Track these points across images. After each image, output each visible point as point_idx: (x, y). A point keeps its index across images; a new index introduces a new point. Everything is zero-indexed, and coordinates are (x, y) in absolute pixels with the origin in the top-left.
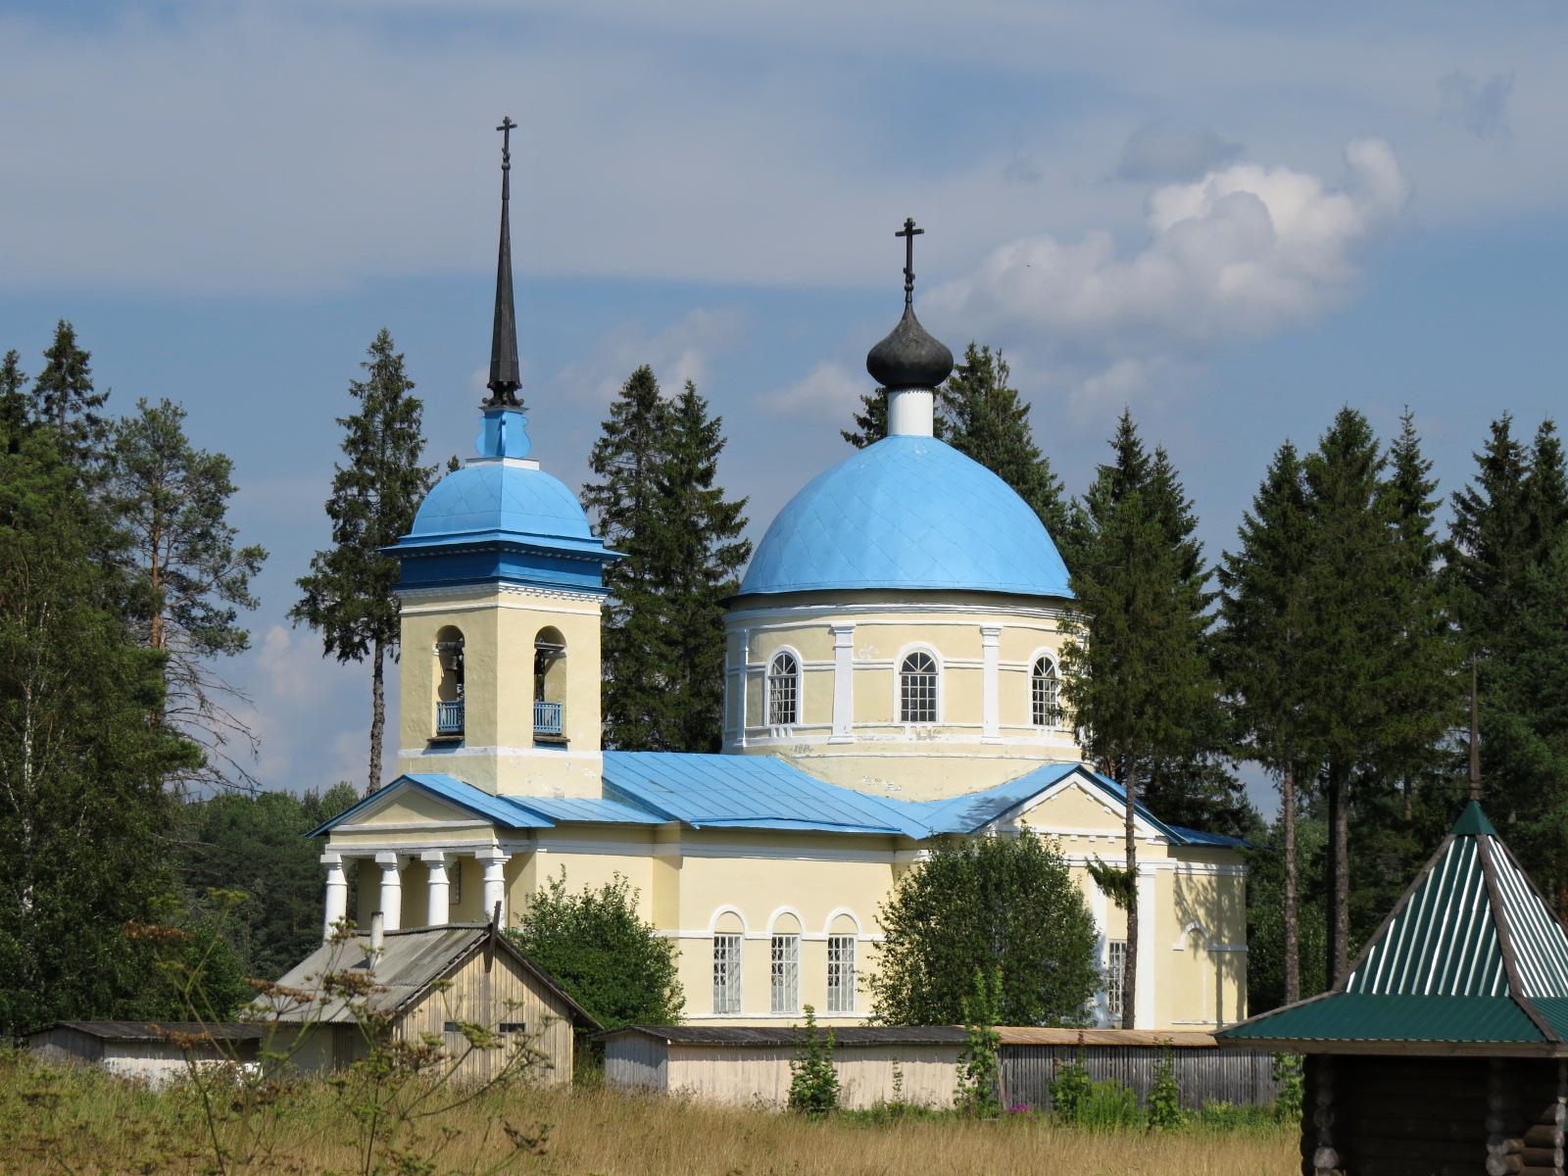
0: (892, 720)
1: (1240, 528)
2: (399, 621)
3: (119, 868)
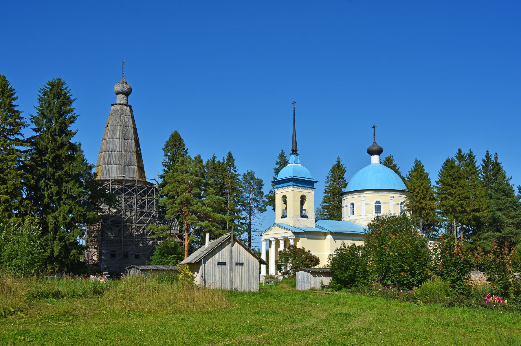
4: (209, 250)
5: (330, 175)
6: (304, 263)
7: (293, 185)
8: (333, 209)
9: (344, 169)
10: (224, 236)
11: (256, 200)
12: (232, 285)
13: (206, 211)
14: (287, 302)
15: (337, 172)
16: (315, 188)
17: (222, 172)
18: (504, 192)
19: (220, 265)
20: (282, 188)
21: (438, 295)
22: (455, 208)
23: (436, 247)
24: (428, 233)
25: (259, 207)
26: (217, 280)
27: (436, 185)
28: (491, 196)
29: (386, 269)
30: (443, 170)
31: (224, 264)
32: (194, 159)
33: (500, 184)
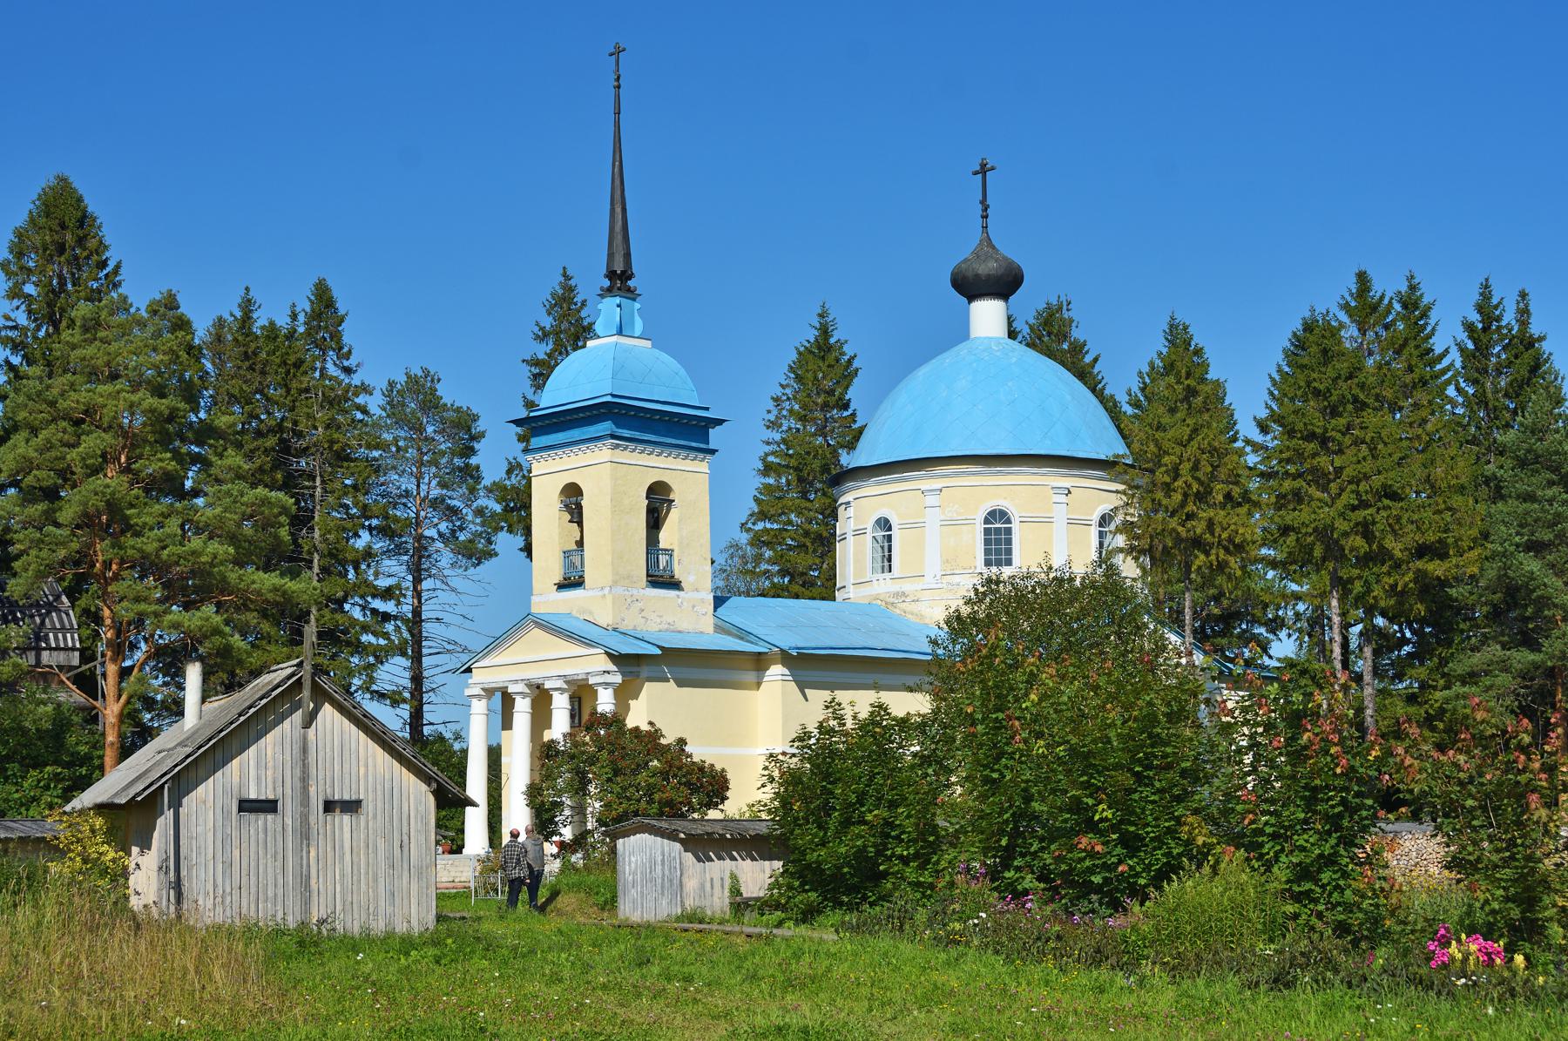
1: (1279, 366)
4: (199, 741)
5: (788, 391)
6: (656, 797)
7: (613, 437)
8: (802, 547)
9: (850, 362)
10: (272, 675)
11: (449, 508)
12: (306, 903)
13: (204, 559)
14: (556, 979)
15: (816, 378)
16: (713, 452)
17: (288, 373)
18: (1556, 470)
19: (251, 811)
20: (560, 452)
21: (1232, 935)
22: (1337, 542)
23: (1228, 719)
24: (1223, 653)
25: (462, 538)
26: (236, 884)
27: (1258, 437)
28: (1499, 488)
29: (1016, 823)
30: (1287, 369)
31: (269, 806)
32: (145, 315)
33: (1537, 431)
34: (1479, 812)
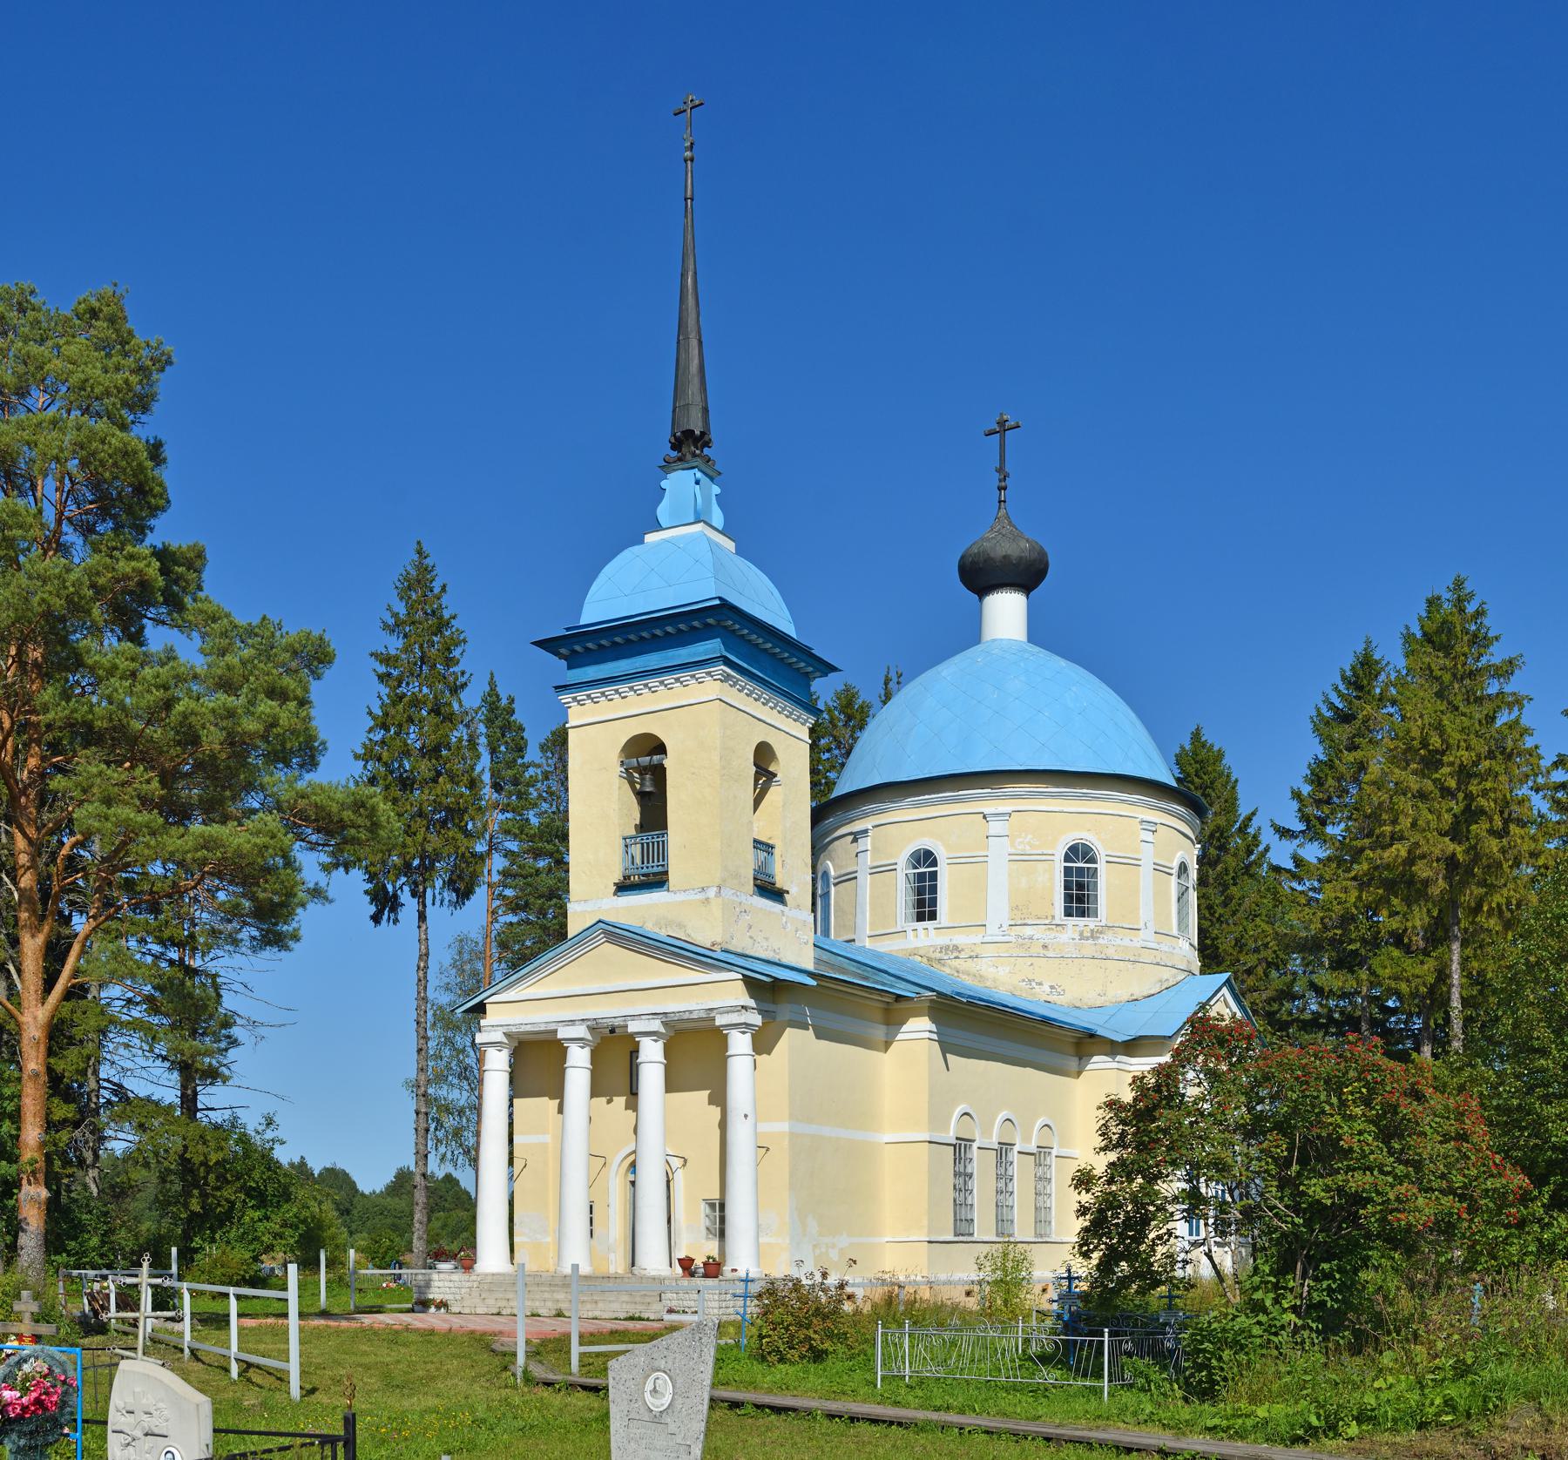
0: (1053, 917)
2: (480, 1061)
3: (124, 927)
34: (731, 1330)
